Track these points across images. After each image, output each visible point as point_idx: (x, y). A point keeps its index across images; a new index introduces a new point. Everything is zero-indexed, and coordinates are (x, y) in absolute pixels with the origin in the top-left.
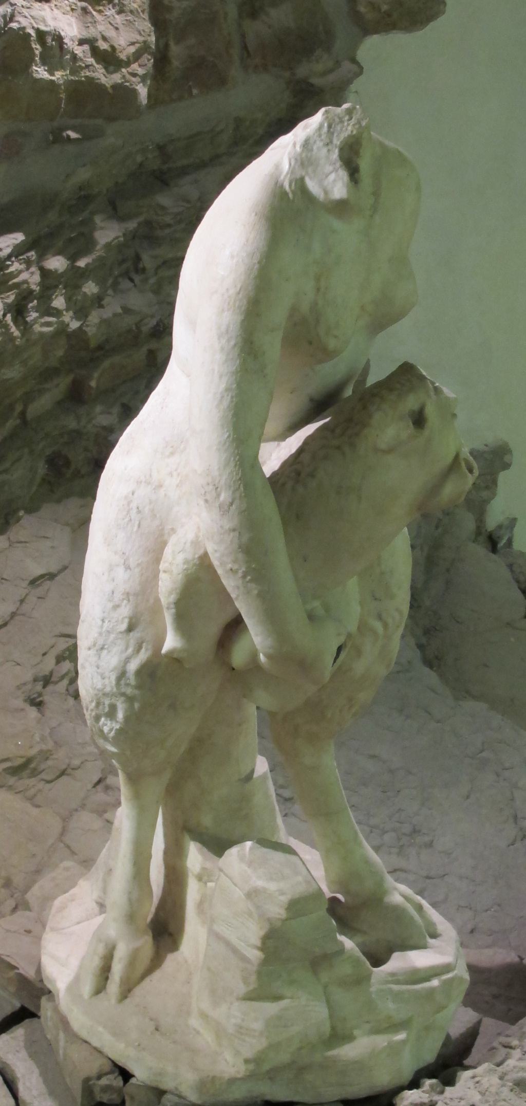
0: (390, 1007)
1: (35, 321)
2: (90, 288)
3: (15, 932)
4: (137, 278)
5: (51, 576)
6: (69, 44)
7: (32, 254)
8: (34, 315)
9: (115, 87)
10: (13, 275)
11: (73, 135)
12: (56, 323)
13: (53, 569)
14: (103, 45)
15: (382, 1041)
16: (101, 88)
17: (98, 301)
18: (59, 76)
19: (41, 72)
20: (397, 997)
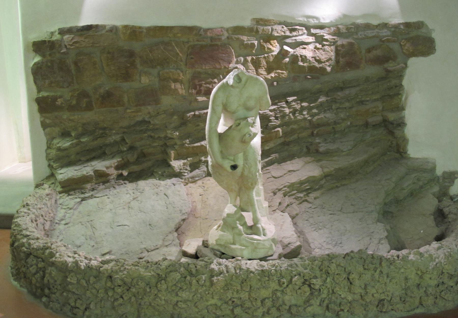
0: (244, 242)
1: (298, 116)
2: (315, 111)
3: (414, 309)
4: (331, 110)
5: (294, 171)
6: (308, 58)
7: (299, 102)
8: (298, 114)
9: (320, 67)
10: (292, 105)
11: (309, 77)
12: (184, 97)
13: (295, 170)
14: (318, 58)
15: (240, 247)
16: (317, 67)
17: (316, 114)
18: (305, 64)
19: (301, 64)
20: (246, 241)
